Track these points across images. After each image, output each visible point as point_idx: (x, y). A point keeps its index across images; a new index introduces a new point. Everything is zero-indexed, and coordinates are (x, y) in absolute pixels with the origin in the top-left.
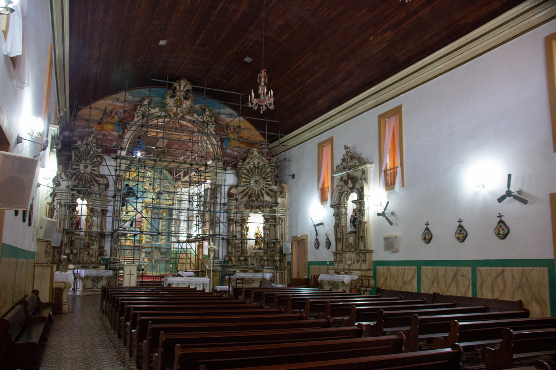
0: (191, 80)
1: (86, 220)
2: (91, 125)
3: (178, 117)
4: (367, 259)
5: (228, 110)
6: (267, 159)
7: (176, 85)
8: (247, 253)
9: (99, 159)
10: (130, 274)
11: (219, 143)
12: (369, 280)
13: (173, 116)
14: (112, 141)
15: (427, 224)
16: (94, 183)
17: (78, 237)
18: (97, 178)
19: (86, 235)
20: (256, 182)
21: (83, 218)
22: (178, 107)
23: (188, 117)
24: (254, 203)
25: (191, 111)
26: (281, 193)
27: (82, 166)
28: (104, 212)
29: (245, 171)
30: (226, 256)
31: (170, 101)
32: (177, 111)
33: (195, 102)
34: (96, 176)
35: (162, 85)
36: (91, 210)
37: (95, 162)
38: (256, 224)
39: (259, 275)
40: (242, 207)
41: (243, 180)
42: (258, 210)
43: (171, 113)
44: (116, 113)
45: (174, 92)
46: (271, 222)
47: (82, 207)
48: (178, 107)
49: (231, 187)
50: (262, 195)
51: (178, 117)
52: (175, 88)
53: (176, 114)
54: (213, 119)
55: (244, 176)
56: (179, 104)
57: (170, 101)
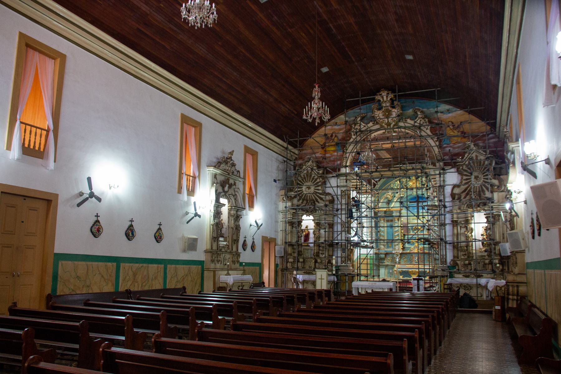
0: (391, 89)
1: (314, 232)
2: (316, 151)
3: (392, 126)
4: (519, 261)
5: (444, 107)
6: (484, 151)
7: (378, 97)
8: (473, 257)
9: (321, 179)
10: (321, 279)
11: (437, 143)
12: (518, 286)
13: (386, 126)
14: (334, 161)
15: (160, 225)
16: (319, 200)
17: (308, 248)
18: (322, 196)
19: (315, 246)
20: (476, 178)
21: (311, 231)
22: (387, 117)
23: (401, 124)
24: (482, 202)
25: (401, 117)
26: (498, 187)
27: (304, 188)
28: (331, 226)
29: (465, 167)
30: (452, 260)
31: (379, 114)
32: (388, 121)
33: (403, 108)
34: (321, 194)
35: (364, 102)
36: (318, 225)
37: (318, 183)
38: (479, 224)
39: (472, 281)
40: (464, 207)
41: (465, 177)
42: (479, 208)
43: (384, 124)
44: (336, 136)
45: (380, 105)
46: (492, 219)
47: (308, 222)
48: (387, 117)
49: (455, 186)
50: (483, 191)
51: (392, 126)
52: (379, 101)
53: (389, 124)
54: (427, 120)
55: (465, 173)
56: (388, 114)
57: (379, 114)
